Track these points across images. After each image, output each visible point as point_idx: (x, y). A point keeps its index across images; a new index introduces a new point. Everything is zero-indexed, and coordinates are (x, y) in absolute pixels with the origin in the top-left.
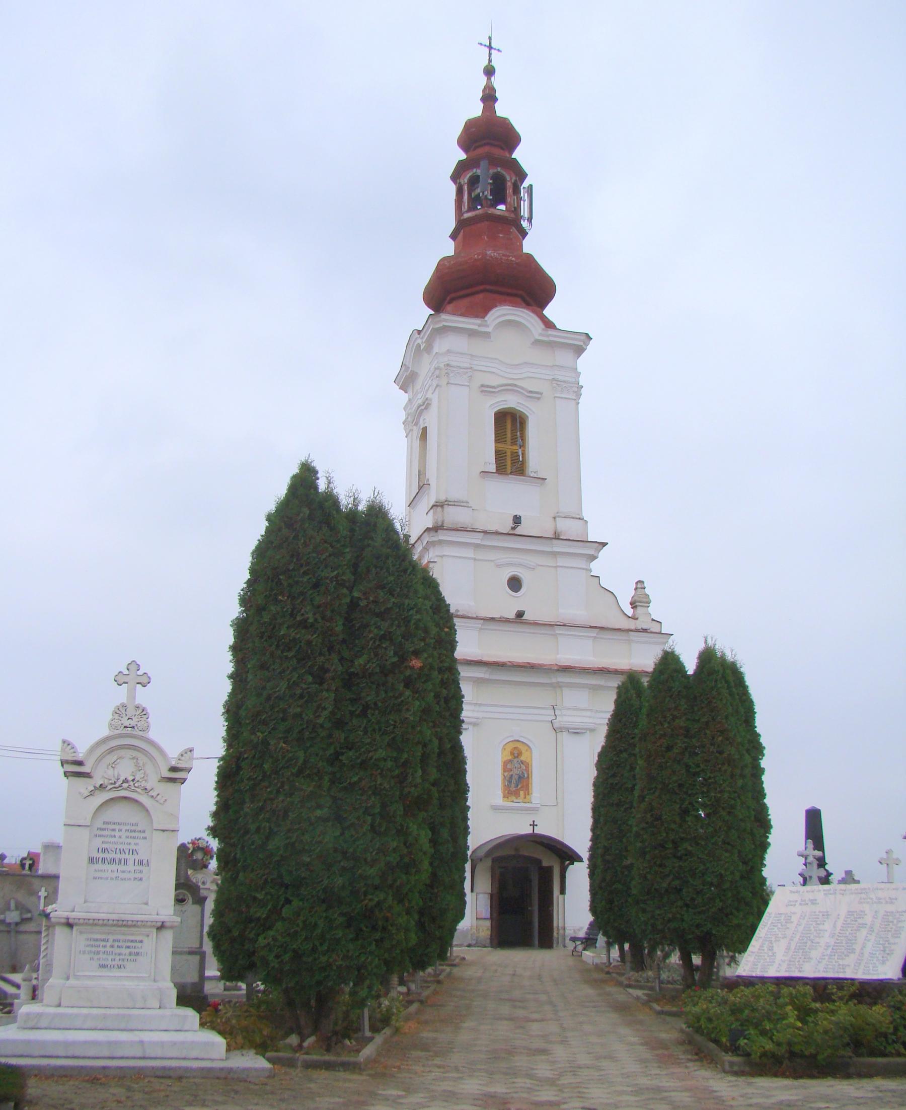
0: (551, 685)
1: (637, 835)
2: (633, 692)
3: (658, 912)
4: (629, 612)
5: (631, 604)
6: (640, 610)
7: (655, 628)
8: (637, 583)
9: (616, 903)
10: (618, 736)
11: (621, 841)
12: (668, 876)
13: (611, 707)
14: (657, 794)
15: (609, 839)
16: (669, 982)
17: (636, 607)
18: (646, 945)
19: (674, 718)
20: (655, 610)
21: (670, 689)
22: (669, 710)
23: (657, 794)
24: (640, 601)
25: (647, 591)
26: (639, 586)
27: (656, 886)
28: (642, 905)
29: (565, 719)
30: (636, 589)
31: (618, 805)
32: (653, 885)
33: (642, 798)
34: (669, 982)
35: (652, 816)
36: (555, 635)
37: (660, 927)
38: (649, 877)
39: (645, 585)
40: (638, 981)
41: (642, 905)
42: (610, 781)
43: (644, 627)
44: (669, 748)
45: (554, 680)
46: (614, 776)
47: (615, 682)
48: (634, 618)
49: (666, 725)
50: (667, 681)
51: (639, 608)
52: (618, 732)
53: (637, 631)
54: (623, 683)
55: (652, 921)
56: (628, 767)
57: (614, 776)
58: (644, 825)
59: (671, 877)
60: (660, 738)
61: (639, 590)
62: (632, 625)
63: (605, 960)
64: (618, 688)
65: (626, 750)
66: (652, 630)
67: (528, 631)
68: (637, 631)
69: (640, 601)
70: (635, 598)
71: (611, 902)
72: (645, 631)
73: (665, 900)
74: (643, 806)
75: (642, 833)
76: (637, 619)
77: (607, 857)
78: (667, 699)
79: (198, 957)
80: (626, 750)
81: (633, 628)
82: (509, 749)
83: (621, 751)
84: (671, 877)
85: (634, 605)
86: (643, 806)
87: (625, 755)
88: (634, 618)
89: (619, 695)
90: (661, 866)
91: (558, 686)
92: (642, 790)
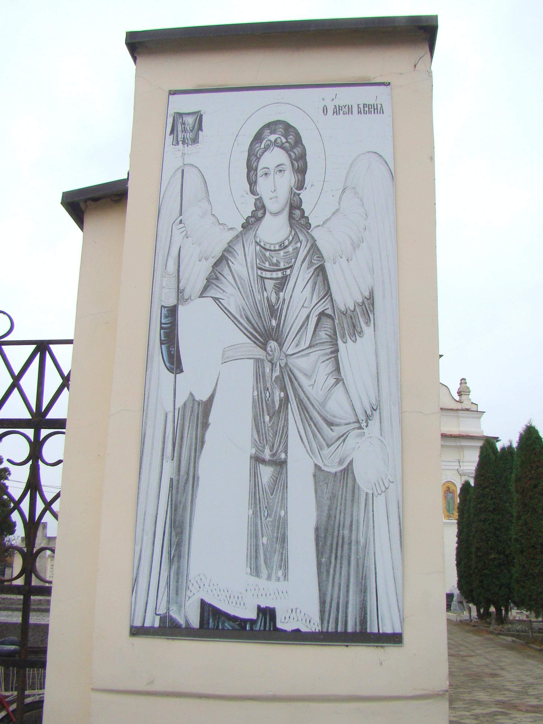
0: (457, 447)
1: (517, 540)
2: (490, 450)
3: (533, 587)
4: (457, 398)
5: (458, 393)
6: (464, 397)
7: (473, 408)
8: (461, 380)
9: (485, 582)
10: (483, 478)
11: (487, 543)
12: (538, 565)
13: (477, 459)
14: (529, 514)
15: (479, 542)
16: (522, 631)
17: (461, 395)
18: (502, 608)
19: (538, 467)
20: (473, 397)
21: (534, 449)
22: (534, 462)
23: (529, 514)
24: (463, 391)
25: (468, 385)
26: (463, 381)
27: (530, 571)
28: (521, 584)
29: (465, 468)
30: (461, 384)
31: (484, 521)
32: (529, 570)
33: (519, 518)
34: (522, 631)
35: (526, 528)
36: (458, 417)
37: (534, 597)
38: (526, 566)
39: (467, 381)
40: (501, 631)
41: (521, 584)
42: (479, 506)
43: (467, 407)
44: (535, 486)
45: (458, 444)
46: (481, 502)
47: (480, 444)
48: (460, 402)
49: (533, 472)
50: (532, 445)
51: (463, 396)
52: (483, 476)
53: (462, 410)
54: (484, 445)
55: (529, 593)
56: (490, 498)
57: (481, 502)
58: (520, 534)
59: (541, 566)
60: (529, 480)
61: (463, 385)
62: (459, 406)
63: (468, 618)
64: (481, 448)
65: (488, 487)
66: (472, 409)
67: (451, 414)
68: (462, 410)
69: (463, 391)
70: (461, 389)
71: (482, 582)
72: (467, 410)
73: (536, 580)
74: (520, 522)
75: (520, 539)
76: (462, 402)
77: (479, 554)
78: (533, 456)
79: (157, 613)
80: (488, 487)
81: (460, 408)
82: (445, 487)
83: (485, 488)
84: (541, 566)
85: (460, 393)
86: (520, 522)
87: (487, 490)
88: (460, 402)
89: (482, 453)
90: (533, 559)
91: (462, 447)
92: (518, 512)
